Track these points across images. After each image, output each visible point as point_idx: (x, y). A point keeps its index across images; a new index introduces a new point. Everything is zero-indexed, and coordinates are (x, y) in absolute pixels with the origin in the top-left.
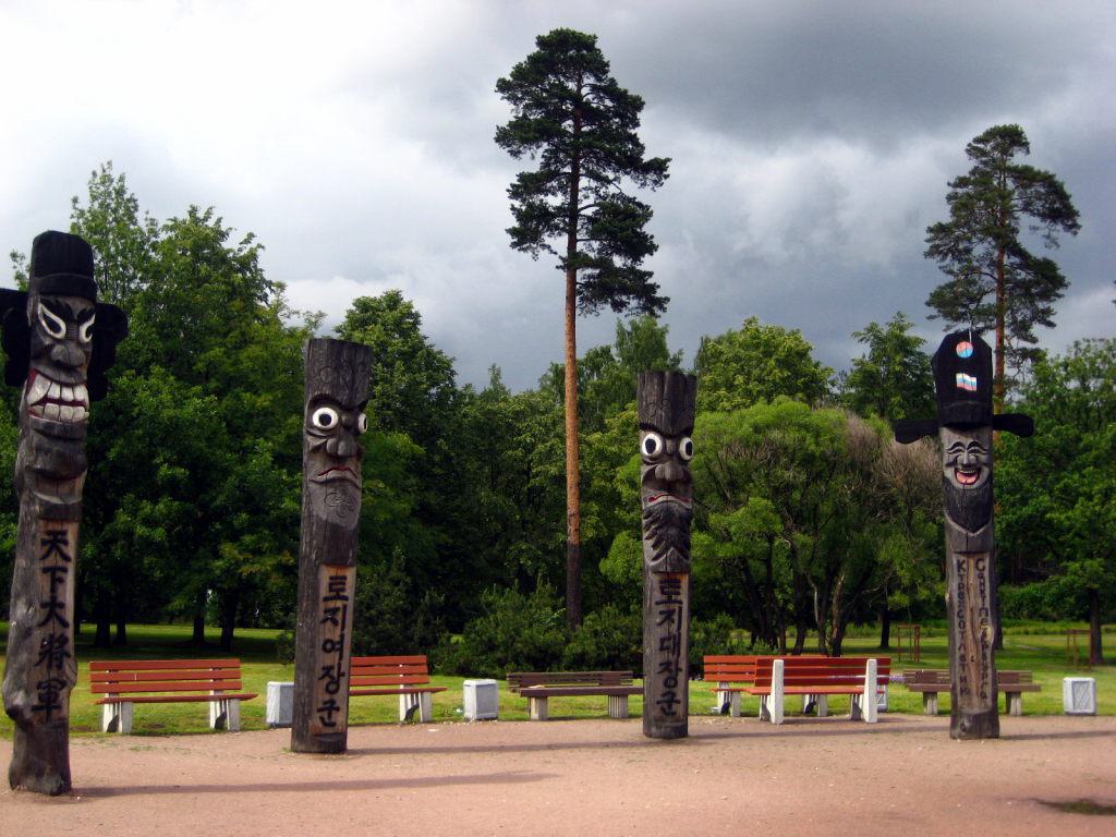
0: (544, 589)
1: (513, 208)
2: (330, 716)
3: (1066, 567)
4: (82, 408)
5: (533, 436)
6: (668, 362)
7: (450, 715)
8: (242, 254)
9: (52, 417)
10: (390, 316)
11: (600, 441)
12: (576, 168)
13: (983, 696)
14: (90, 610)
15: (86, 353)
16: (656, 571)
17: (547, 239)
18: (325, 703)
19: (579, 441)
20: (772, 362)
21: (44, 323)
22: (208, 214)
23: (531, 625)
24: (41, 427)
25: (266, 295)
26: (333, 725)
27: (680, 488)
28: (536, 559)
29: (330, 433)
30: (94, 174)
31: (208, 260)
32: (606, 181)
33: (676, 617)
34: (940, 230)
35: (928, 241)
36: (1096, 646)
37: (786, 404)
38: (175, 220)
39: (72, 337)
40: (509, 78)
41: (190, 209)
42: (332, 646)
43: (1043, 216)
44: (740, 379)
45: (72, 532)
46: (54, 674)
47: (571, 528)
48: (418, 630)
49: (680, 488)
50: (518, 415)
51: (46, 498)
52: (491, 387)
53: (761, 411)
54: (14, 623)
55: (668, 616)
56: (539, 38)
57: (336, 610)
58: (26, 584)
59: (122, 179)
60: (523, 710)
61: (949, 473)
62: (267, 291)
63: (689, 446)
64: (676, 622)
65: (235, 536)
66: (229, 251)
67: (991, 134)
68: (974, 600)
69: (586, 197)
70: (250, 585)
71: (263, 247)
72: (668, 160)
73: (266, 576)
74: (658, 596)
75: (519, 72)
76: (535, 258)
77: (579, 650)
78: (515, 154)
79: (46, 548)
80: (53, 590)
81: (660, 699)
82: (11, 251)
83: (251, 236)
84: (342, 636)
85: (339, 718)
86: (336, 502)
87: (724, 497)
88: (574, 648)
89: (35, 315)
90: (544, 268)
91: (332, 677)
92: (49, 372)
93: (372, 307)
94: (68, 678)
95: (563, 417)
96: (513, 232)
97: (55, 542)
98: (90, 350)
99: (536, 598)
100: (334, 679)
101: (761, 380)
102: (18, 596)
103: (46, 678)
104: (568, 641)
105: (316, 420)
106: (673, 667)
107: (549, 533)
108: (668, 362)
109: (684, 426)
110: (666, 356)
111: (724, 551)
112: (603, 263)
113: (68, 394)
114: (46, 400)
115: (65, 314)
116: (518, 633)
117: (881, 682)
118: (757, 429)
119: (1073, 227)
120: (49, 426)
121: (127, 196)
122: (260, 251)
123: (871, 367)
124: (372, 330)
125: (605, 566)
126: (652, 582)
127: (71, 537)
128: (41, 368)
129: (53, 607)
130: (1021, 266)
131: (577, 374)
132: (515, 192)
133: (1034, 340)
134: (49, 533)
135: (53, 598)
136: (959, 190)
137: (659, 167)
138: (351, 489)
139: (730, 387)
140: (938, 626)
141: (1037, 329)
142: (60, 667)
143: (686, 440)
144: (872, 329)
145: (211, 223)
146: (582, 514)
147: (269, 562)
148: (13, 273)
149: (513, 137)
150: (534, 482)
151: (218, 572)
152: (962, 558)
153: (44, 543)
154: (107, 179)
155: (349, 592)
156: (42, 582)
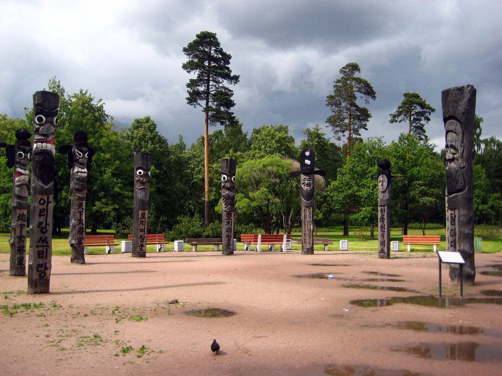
0: (197, 215)
1: (188, 91)
3: (361, 209)
5: (194, 165)
6: (243, 136)
7: (172, 250)
10: (147, 125)
11: (216, 167)
12: (209, 77)
13: (310, 243)
14: (369, 209)
16: (225, 211)
17: (199, 101)
19: (209, 167)
20: (274, 141)
22: (86, 92)
23: (193, 227)
26: (142, 250)
27: (232, 189)
28: (195, 206)
29: (141, 176)
30: (50, 80)
31: (87, 108)
32: (218, 82)
34: (331, 97)
35: (327, 101)
36: (372, 235)
37: (276, 157)
39: (84, 157)
40: (187, 47)
42: (142, 230)
43: (365, 94)
44: (263, 146)
46: (81, 236)
47: (206, 196)
48: (159, 228)
49: (232, 189)
50: (189, 158)
52: (180, 143)
53: (267, 160)
55: (228, 223)
56: (197, 35)
57: (143, 221)
58: (74, 215)
60: (190, 249)
61: (303, 186)
62: (106, 118)
63: (234, 179)
68: (308, 219)
69: (212, 88)
70: (104, 215)
72: (239, 76)
73: (110, 212)
74: (226, 218)
75: (190, 45)
76: (195, 107)
77: (208, 234)
78: (189, 72)
80: (80, 216)
83: (101, 100)
85: (144, 248)
86: (143, 194)
87: (253, 187)
88: (206, 233)
89: (75, 151)
90: (198, 112)
92: (78, 165)
93: (140, 122)
95: (204, 159)
96: (188, 99)
97: (80, 205)
99: (194, 219)
100: (142, 239)
101: (270, 147)
102: (72, 218)
104: (204, 231)
105: (138, 173)
107: (199, 197)
108: (243, 136)
109: (233, 173)
110: (242, 134)
111: (254, 204)
112: (218, 111)
113: (83, 170)
114: (78, 172)
115: (82, 151)
116: (189, 229)
117: (287, 241)
118: (264, 166)
119: (374, 97)
120: (79, 178)
121: (61, 88)
122: (104, 105)
123: (307, 143)
124: (141, 130)
125: (216, 209)
126: (224, 214)
127: (84, 204)
129: (80, 220)
130: (356, 110)
131: (209, 140)
132: (189, 86)
133: (360, 135)
134: (79, 203)
136: (338, 84)
137: (236, 79)
138: (147, 191)
139: (260, 149)
140: (334, 229)
141: (362, 131)
142: (82, 234)
143: (234, 177)
144: (308, 130)
145: (88, 95)
146: (210, 191)
147: (111, 207)
149: (188, 67)
150: (195, 180)
151: (95, 211)
152: (305, 208)
153: (78, 205)
154: (54, 82)
155: (146, 217)
156: (78, 215)
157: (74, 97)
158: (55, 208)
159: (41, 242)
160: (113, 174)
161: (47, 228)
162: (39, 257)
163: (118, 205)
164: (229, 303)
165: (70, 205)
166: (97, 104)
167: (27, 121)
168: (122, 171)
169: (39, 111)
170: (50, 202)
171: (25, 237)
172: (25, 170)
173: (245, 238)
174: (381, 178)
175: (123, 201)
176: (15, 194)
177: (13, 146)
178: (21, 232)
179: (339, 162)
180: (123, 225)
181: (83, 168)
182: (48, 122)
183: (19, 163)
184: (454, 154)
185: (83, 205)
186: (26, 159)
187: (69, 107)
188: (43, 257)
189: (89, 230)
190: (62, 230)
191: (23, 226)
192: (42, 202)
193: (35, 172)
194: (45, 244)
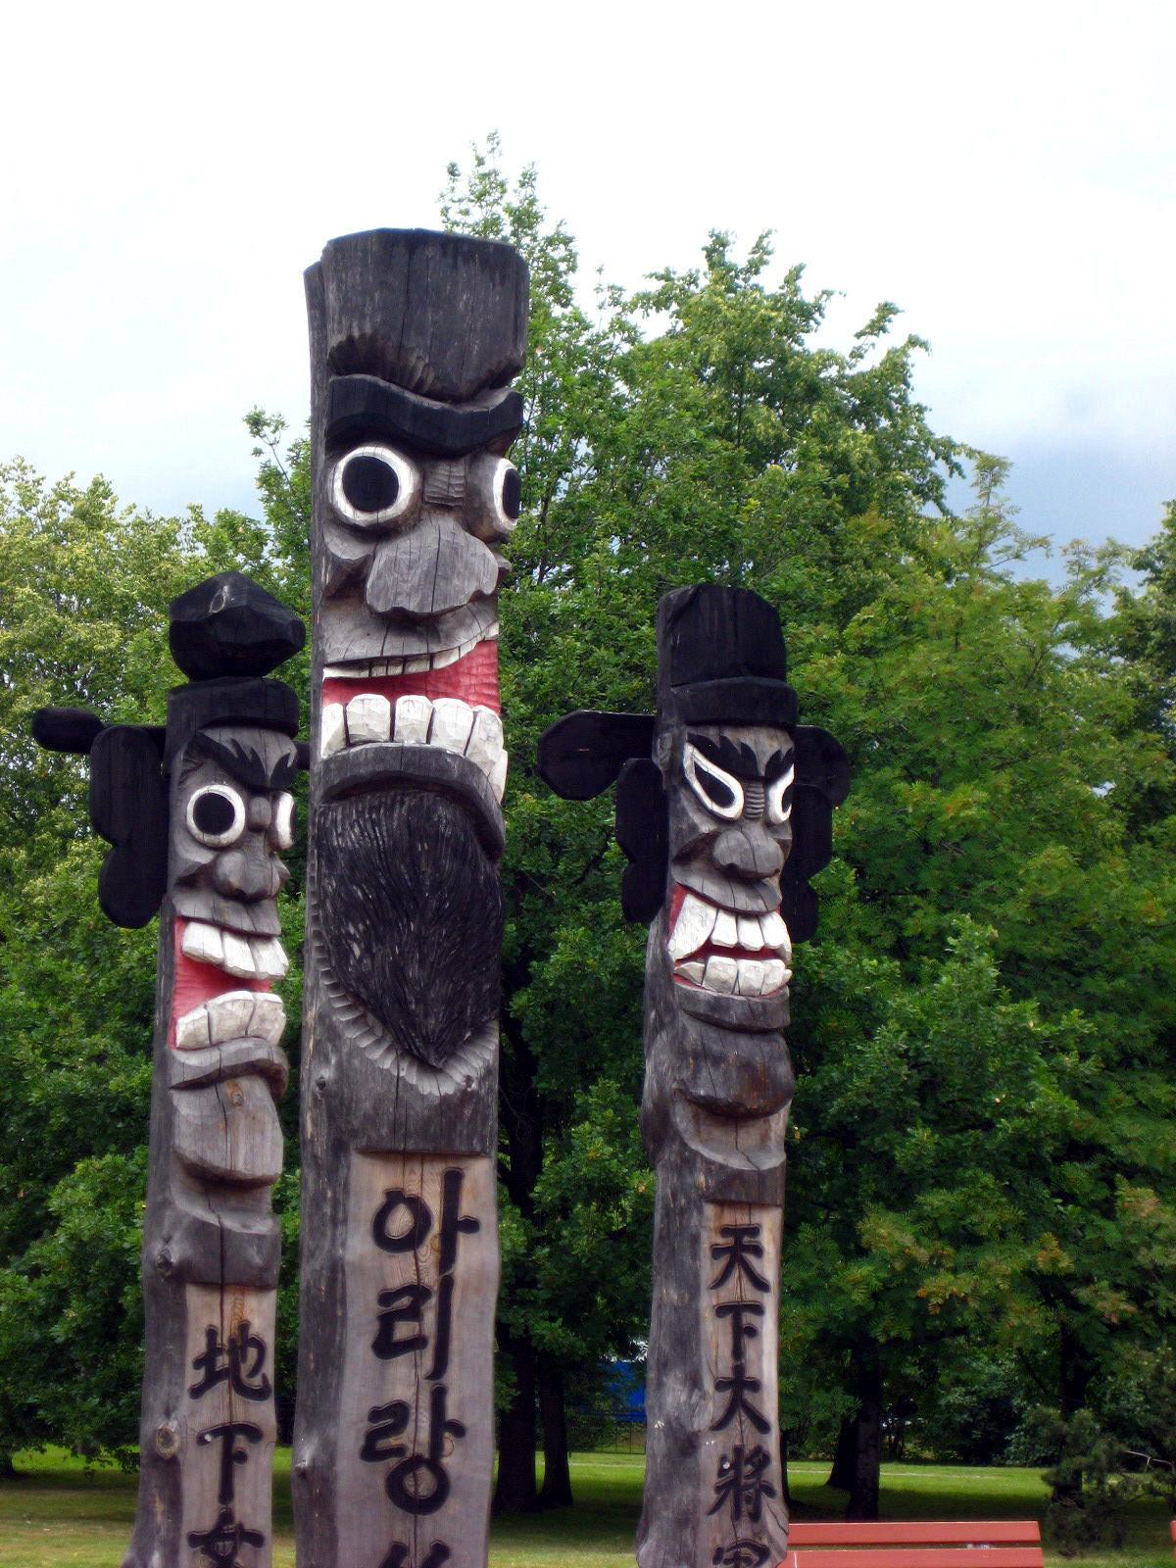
4: (778, 963)
8: (865, 366)
9: (723, 985)
15: (783, 844)
21: (697, 786)
24: (702, 1009)
25: (938, 483)
30: (453, 171)
38: (666, 277)
41: (709, 242)
45: (769, 1225)
46: (744, 1531)
51: (718, 1158)
54: (660, 1424)
59: (527, 180)
62: (940, 468)
65: (900, 1194)
66: (828, 359)
71: (924, 345)
80: (738, 1352)
82: (250, 410)
83: (886, 311)
89: (675, 767)
92: (712, 890)
94: (771, 1540)
97: (739, 1249)
98: (788, 836)
102: (664, 1366)
103: (728, 1543)
113: (751, 935)
114: (709, 949)
120: (717, 1004)
121: (544, 230)
122: (915, 355)
127: (769, 1239)
128: (695, 882)
129: (740, 1385)
134: (725, 1231)
135: (739, 1369)
142: (756, 1516)
145: (770, 281)
147: (1002, 1264)
148: (253, 469)
151: (858, 1297)
157: (661, 302)
158: (517, 1279)
160: (1011, 962)
161: (450, 1462)
163: (1064, 1237)
164: (427, 576)
165: (647, 1244)
166: (857, 354)
167: (270, 530)
168: (1096, 941)
169: (359, 408)
170: (472, 1226)
171: (256, 1539)
172: (252, 937)
175: (1108, 1209)
177: (156, 735)
178: (226, 1492)
180: (1117, 1425)
182: (443, 506)
183: (200, 880)
185: (758, 1251)
186: (259, 842)
187: (621, 388)
189: (813, 1473)
190: (584, 1467)
191: (241, 1442)
192: (400, 1222)
193: (337, 951)
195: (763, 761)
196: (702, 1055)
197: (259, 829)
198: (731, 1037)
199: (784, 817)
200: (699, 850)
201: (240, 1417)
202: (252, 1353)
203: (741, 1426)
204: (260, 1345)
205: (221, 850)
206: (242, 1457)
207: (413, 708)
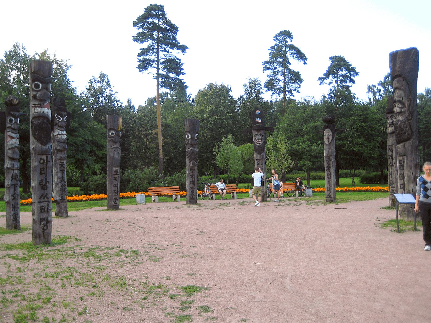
2: (116, 202)
9: (60, 138)
18: (115, 198)
21: (56, 118)
26: (117, 203)
33: (194, 176)
39: (63, 120)
55: (192, 176)
64: (194, 177)
67: (281, 33)
79: (60, 166)
81: (190, 195)
84: (118, 183)
91: (116, 193)
92: (58, 128)
106: (193, 188)
112: (167, 77)
113: (63, 133)
114: (58, 134)
128: (57, 128)
129: (63, 178)
132: (140, 55)
134: (61, 163)
135: (62, 176)
137: (183, 48)
149: (140, 38)
159: (43, 198)
162: (41, 212)
170: (49, 161)
173: (152, 190)
174: (326, 132)
176: (8, 156)
179: (275, 121)
181: (62, 131)
184: (401, 108)
185: (64, 165)
188: (44, 212)
192: (42, 161)
194: (46, 200)
195: (63, 115)
196: (58, 145)
197: (16, 122)
198: (61, 143)
199: (66, 121)
200: (57, 124)
201: (16, 183)
202: (17, 176)
203: (63, 182)
204: (17, 175)
205: (12, 124)
206: (16, 187)
207: (42, 109)
